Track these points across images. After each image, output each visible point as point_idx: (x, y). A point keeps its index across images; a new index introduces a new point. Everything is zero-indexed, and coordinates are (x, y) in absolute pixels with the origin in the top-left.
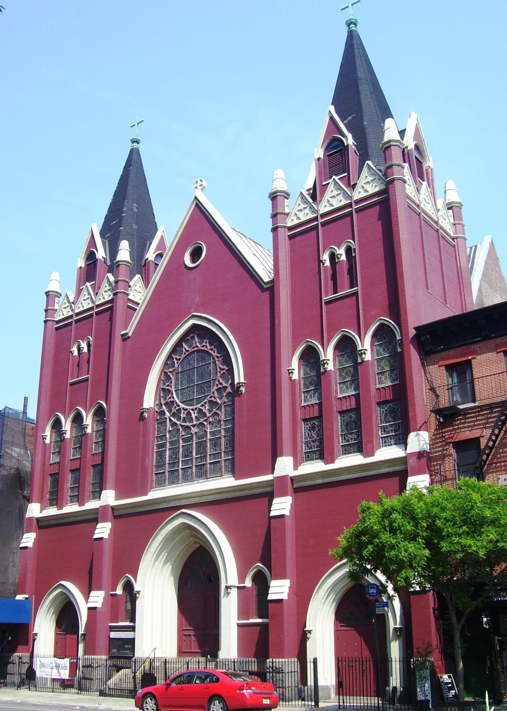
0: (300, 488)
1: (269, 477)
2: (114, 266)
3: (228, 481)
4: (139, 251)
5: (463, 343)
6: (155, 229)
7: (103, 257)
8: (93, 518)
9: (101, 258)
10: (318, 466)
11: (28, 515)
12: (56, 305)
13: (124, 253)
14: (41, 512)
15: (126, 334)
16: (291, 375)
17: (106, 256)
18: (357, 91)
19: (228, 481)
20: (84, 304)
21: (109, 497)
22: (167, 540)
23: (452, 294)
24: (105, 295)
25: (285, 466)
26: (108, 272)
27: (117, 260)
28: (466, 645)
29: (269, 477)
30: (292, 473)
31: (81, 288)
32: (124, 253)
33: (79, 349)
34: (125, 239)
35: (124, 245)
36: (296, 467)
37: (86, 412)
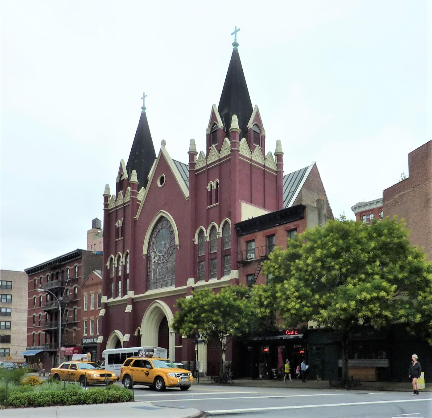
0: (133, 301)
1: (185, 287)
2: (227, 132)
3: (173, 288)
4: (243, 122)
5: (290, 221)
6: (251, 110)
7: (222, 127)
8: (124, 305)
9: (221, 127)
10: (112, 300)
11: (102, 302)
12: (108, 202)
13: (235, 123)
14: (195, 284)
15: (136, 218)
16: (194, 242)
17: (224, 125)
18: (235, 94)
19: (173, 288)
20: (214, 158)
21: (131, 294)
22: (151, 313)
23: (270, 200)
24: (225, 152)
25: (191, 282)
26: (226, 137)
27: (231, 128)
28: (356, 356)
29: (185, 287)
30: (106, 301)
31: (209, 148)
32: (235, 123)
33: (211, 186)
34: (135, 170)
35: (235, 118)
36: (108, 299)
37: (231, 220)
